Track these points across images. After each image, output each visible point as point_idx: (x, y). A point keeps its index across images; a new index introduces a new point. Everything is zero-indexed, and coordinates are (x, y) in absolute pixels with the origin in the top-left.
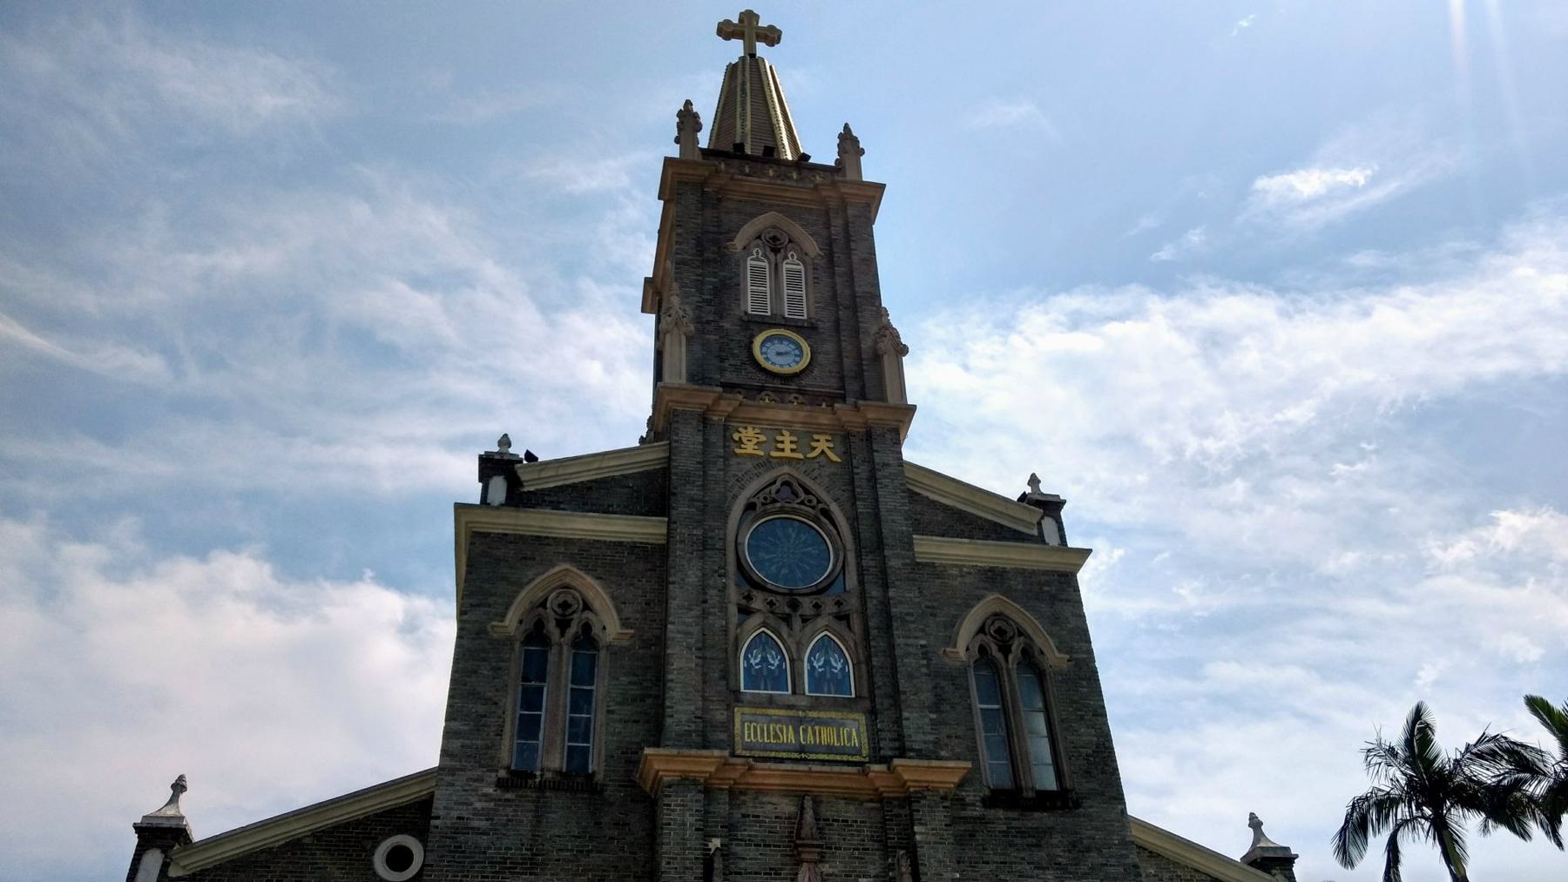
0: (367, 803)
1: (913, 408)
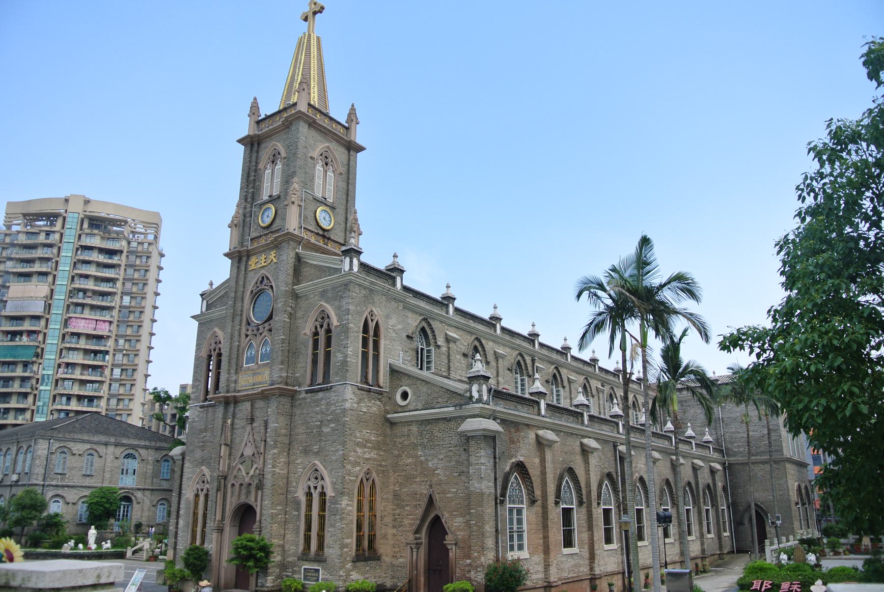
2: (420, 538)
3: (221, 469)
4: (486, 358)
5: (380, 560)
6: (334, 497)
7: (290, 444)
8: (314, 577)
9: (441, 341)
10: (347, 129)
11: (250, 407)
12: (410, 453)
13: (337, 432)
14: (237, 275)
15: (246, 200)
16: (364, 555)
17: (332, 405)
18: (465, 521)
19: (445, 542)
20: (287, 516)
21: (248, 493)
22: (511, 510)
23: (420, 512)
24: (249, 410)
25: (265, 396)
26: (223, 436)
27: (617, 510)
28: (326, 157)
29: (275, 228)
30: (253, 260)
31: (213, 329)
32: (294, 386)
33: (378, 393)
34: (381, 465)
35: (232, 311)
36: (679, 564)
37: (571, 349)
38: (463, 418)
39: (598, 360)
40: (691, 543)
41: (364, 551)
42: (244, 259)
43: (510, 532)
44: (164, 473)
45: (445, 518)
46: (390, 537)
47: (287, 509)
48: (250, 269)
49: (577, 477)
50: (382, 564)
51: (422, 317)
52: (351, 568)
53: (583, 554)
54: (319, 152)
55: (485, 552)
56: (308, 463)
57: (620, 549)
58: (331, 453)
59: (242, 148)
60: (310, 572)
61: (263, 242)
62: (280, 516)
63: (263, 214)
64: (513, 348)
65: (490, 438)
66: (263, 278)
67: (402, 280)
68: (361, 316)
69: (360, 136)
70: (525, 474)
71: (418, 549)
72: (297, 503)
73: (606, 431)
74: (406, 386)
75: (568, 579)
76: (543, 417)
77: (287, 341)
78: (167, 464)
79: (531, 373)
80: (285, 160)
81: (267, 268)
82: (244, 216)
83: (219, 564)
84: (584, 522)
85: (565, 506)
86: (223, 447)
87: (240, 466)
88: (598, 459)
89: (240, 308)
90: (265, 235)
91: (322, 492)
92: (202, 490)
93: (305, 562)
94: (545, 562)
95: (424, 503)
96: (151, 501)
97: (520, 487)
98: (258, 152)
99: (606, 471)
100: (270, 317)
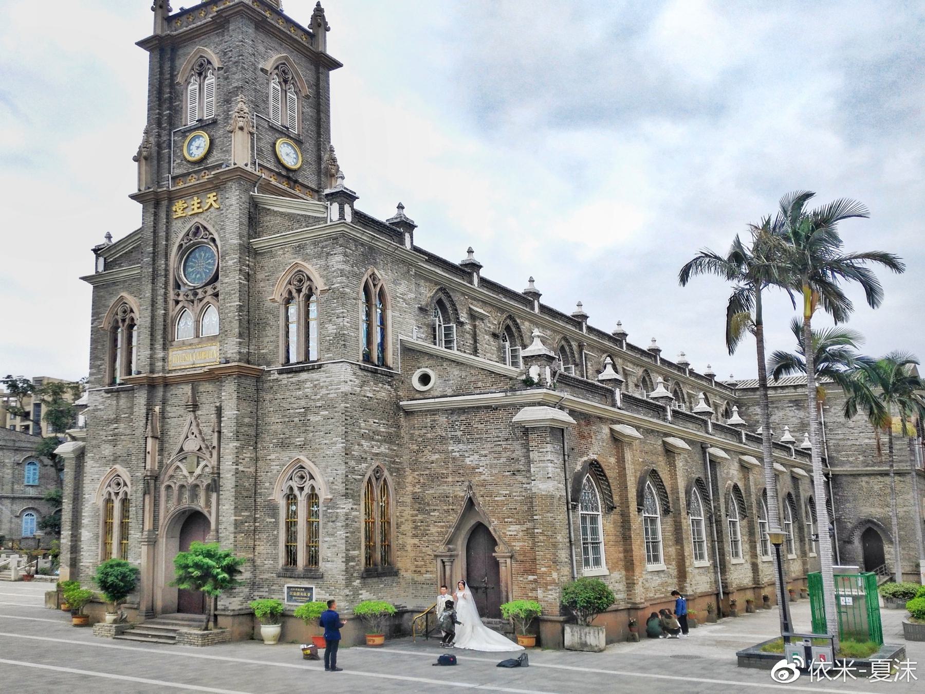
0: (428, 267)
1: (136, 159)
2: (454, 550)
3: (148, 467)
4: (522, 340)
5: (397, 575)
6: (331, 499)
7: (257, 436)
8: (303, 597)
9: (464, 317)
10: (312, 36)
11: (190, 391)
12: (436, 447)
13: (333, 420)
14: (154, 223)
15: (159, 124)
16: (376, 570)
17: (322, 387)
18: (525, 529)
19: (494, 554)
20: (257, 524)
21: (194, 496)
22: (584, 518)
23: (454, 518)
24: (190, 394)
25: (214, 376)
26: (149, 427)
27: (708, 522)
28: (284, 71)
29: (212, 162)
30: (178, 206)
31: (118, 293)
32: (259, 365)
33: (386, 375)
34: (394, 462)
35: (151, 270)
36: (801, 581)
37: (627, 335)
38: (517, 407)
39: (660, 351)
40: (791, 562)
41: (375, 565)
42: (165, 203)
43: (584, 544)
44: (29, 478)
45: (494, 525)
46: (409, 548)
47: (257, 516)
48: (175, 217)
49: (662, 482)
50: (401, 580)
51: (438, 287)
52: (360, 586)
53: (671, 571)
54: (274, 64)
55: (558, 567)
56: (287, 459)
57: (712, 567)
58: (325, 447)
59: (145, 55)
60: (297, 592)
61: (193, 181)
62: (246, 524)
63: (190, 144)
64: (555, 331)
65: (557, 432)
66: (198, 228)
67: (412, 237)
68: (360, 279)
69: (333, 47)
70: (600, 475)
71: (452, 562)
72: (273, 510)
73: (693, 430)
74: (427, 367)
75: (655, 599)
76: (619, 409)
77: (246, 309)
78: (32, 467)
79: (578, 361)
80: (221, 72)
81: (203, 216)
82: (159, 145)
83: (153, 586)
84: (670, 534)
85: (647, 515)
86: (150, 440)
87: (179, 464)
88: (684, 463)
89: (163, 266)
90: (195, 172)
91: (313, 495)
92: (117, 494)
93: (291, 580)
94: (627, 579)
95: (460, 509)
96: (12, 512)
97: (594, 490)
98: (172, 60)
99: (696, 476)
100: (215, 278)
